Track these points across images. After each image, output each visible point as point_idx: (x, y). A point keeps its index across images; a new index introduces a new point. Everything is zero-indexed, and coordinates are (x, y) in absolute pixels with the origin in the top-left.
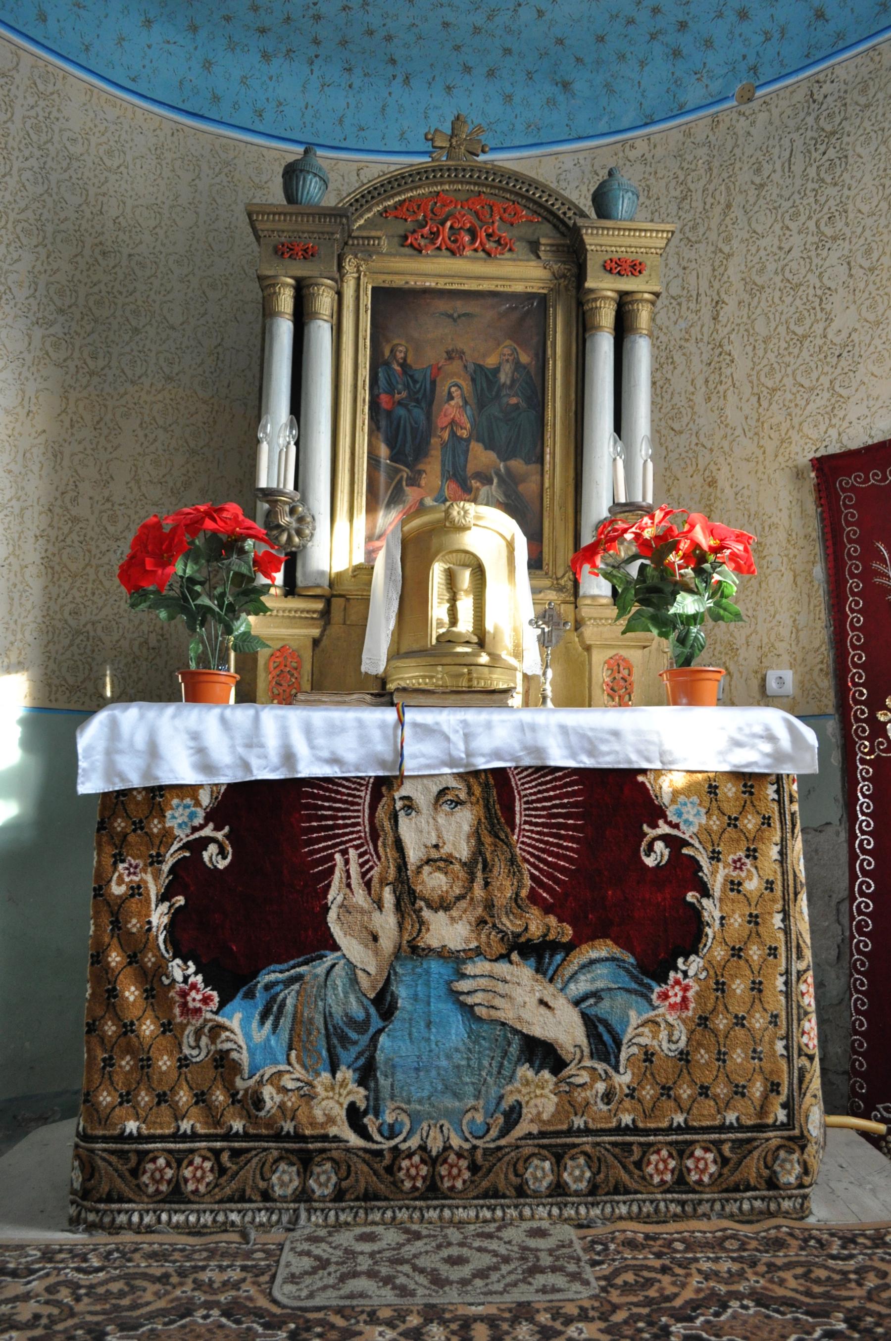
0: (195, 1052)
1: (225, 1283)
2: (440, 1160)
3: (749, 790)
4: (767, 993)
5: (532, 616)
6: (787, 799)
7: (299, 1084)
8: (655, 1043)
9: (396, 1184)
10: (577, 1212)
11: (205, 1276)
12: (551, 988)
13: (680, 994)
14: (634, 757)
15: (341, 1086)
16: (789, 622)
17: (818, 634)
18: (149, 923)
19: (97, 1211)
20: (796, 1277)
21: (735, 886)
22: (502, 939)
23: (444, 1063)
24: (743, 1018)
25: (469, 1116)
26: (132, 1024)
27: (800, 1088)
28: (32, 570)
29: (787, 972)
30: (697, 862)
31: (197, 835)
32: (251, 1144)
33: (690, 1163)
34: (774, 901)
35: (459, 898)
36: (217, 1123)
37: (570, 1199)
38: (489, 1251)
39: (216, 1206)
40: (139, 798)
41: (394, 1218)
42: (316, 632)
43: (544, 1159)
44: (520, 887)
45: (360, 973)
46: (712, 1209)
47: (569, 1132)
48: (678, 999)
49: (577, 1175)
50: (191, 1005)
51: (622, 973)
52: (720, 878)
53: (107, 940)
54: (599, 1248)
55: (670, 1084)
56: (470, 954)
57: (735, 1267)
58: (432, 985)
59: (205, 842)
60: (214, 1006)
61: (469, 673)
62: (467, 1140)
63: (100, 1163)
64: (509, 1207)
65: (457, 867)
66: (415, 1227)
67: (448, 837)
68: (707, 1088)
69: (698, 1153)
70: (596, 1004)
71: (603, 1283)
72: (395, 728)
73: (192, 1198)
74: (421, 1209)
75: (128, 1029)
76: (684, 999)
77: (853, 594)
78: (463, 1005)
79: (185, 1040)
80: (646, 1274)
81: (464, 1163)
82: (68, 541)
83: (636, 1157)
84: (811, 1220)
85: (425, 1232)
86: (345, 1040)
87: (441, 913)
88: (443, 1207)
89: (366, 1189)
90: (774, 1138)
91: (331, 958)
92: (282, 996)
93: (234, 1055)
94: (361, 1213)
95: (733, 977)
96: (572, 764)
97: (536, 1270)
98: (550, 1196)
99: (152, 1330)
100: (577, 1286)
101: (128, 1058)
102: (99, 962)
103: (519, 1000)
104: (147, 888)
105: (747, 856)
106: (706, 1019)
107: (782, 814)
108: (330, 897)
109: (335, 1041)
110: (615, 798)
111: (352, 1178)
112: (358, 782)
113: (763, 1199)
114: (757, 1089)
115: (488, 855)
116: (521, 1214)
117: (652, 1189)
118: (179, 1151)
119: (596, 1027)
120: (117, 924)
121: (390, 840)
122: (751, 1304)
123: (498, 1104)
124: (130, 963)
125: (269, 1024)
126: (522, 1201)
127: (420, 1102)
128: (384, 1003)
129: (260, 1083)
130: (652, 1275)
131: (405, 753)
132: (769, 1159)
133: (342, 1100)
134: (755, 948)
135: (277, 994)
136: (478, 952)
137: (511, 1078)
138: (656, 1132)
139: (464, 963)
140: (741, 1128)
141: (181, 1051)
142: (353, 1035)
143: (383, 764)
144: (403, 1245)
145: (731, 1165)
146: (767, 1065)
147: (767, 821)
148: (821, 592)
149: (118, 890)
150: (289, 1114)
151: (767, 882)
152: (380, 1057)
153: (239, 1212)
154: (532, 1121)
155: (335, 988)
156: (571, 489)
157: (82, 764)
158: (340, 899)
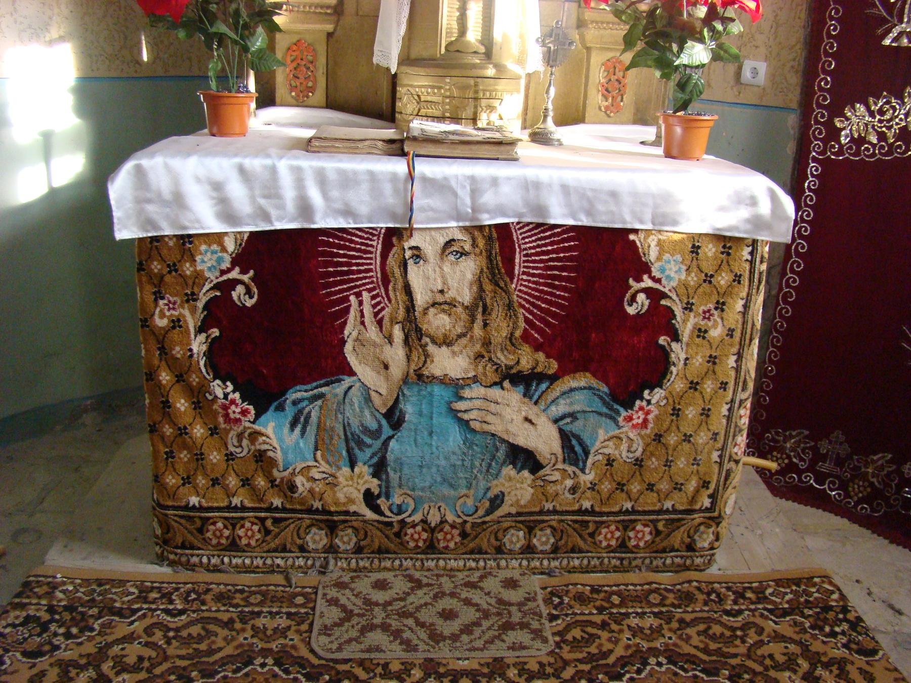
1: (275, 630)
2: (438, 529)
6: (758, 260)
7: (325, 476)
8: (617, 452)
9: (404, 545)
10: (541, 564)
11: (260, 622)
12: (535, 409)
13: (642, 417)
14: (628, 217)
18: (191, 350)
19: (176, 554)
20: (699, 633)
21: (701, 333)
22: (497, 370)
23: (443, 462)
24: (691, 436)
25: (462, 500)
26: (185, 428)
27: (725, 484)
30: (673, 311)
31: (225, 277)
32: (289, 515)
33: (632, 534)
34: (731, 345)
35: (460, 336)
36: (261, 500)
37: (536, 556)
39: (264, 555)
40: (171, 243)
41: (401, 565)
42: (330, 27)
44: (515, 328)
45: (373, 394)
46: (643, 563)
47: (541, 513)
48: (640, 421)
49: (543, 540)
50: (232, 416)
52: (689, 326)
53: (156, 362)
55: (625, 481)
56: (468, 382)
57: (656, 622)
58: (435, 404)
59: (234, 283)
60: (251, 416)
61: (476, 85)
62: (459, 517)
63: (173, 523)
64: (489, 560)
65: (460, 310)
66: (417, 575)
67: (453, 283)
68: (653, 485)
69: (639, 527)
70: (572, 422)
71: (557, 639)
72: (406, 181)
73: (246, 548)
74: (422, 560)
75: (182, 431)
76: (645, 421)
78: (460, 420)
79: (229, 441)
80: (589, 629)
81: (456, 532)
83: (591, 530)
84: (713, 570)
85: (425, 581)
86: (361, 444)
87: (444, 348)
88: (438, 559)
89: (380, 547)
90: (698, 518)
91: (348, 381)
92: (307, 410)
93: (270, 454)
94: (376, 561)
95: (688, 405)
96: (571, 222)
97: (508, 626)
98: (522, 553)
99: (225, 677)
100: (538, 644)
104: (185, 321)
105: (716, 309)
106: (661, 436)
107: (752, 272)
108: (346, 333)
109: (353, 444)
110: (603, 255)
111: (369, 539)
112: (371, 233)
113: (682, 557)
115: (488, 301)
116: (498, 565)
117: (600, 550)
118: (233, 518)
119: (570, 441)
120: (164, 351)
121: (400, 285)
122: (664, 661)
123: (485, 493)
124: (178, 381)
126: (499, 556)
127: (423, 489)
128: (394, 417)
129: (293, 474)
130: (595, 631)
132: (692, 531)
133: (359, 487)
134: (709, 382)
135: (304, 408)
136: (475, 379)
137: (497, 476)
138: (609, 514)
139: (463, 387)
140: (675, 511)
141: (227, 449)
142: (368, 440)
143: (394, 217)
144: (408, 594)
145: (662, 536)
146: (702, 469)
147: (738, 279)
150: (317, 496)
151: (729, 329)
152: (390, 457)
153: (283, 558)
154: (512, 505)
155: (352, 404)
157: (117, 214)
158: (355, 334)
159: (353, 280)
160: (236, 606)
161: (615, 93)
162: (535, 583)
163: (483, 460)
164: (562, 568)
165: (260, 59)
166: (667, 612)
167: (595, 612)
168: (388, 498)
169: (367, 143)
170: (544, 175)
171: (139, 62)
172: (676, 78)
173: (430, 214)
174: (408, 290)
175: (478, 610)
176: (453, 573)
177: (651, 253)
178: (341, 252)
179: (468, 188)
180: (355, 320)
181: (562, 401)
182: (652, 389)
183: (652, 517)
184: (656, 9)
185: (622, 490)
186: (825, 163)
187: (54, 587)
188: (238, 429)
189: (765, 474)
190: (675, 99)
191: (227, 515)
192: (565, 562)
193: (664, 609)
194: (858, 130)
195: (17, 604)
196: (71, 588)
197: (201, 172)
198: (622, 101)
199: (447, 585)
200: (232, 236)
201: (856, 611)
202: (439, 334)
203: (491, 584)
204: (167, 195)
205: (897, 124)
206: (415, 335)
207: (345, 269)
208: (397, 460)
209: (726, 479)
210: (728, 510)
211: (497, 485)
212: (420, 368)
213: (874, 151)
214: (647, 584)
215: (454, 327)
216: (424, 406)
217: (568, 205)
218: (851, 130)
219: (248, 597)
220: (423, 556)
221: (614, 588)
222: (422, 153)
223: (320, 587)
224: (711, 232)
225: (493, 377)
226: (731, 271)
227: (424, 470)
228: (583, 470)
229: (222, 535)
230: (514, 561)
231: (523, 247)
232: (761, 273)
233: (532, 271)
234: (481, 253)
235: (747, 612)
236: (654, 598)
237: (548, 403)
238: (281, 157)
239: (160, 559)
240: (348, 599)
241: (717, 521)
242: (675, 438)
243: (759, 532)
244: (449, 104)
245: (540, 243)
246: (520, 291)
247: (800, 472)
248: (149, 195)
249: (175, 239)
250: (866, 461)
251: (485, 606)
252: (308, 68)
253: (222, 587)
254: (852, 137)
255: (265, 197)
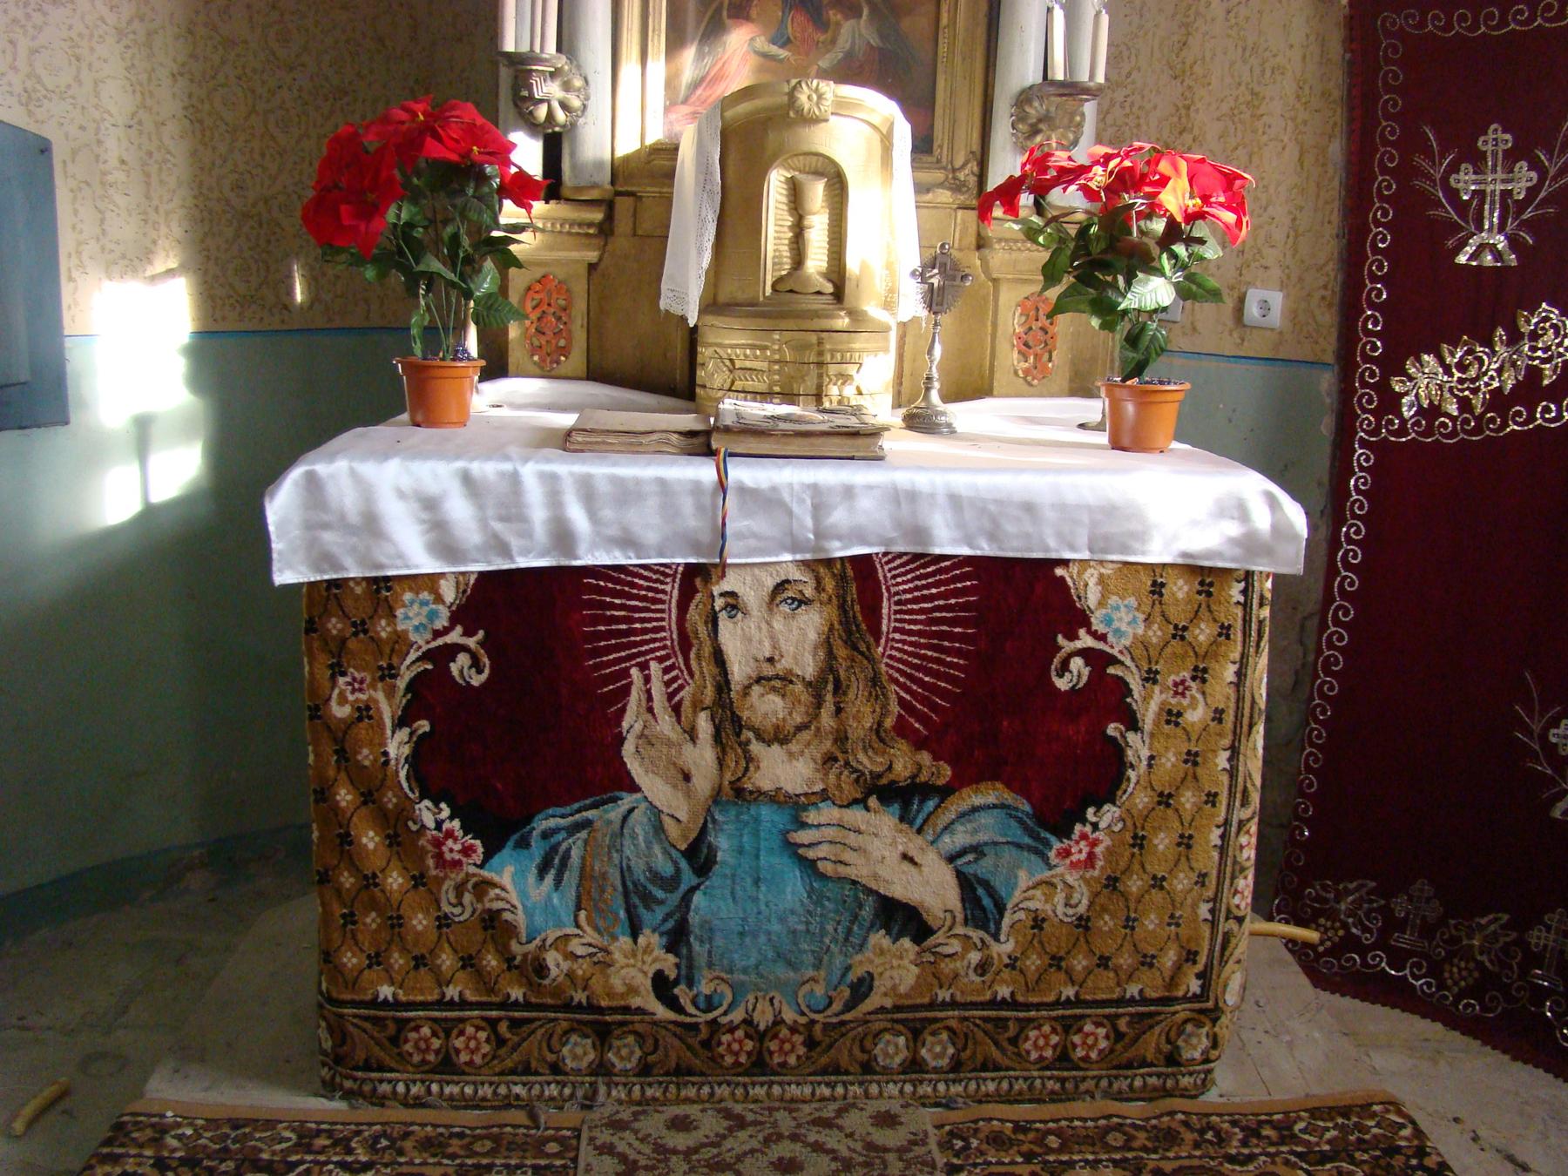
0: (457, 910)
2: (770, 1035)
3: (1206, 590)
4: (1196, 848)
5: (915, 262)
6: (1255, 602)
8: (1048, 907)
9: (716, 1060)
10: (935, 1089)
12: (919, 840)
13: (1086, 850)
14: (1052, 542)
15: (645, 952)
16: (1287, 221)
17: (1326, 247)
18: (386, 754)
19: (355, 1079)
21: (1172, 716)
22: (857, 781)
23: (776, 927)
25: (807, 987)
26: (375, 876)
27: (1222, 954)
28: (172, 128)
29: (1227, 823)
30: (1126, 684)
31: (440, 642)
32: (534, 1014)
33: (1077, 1039)
34: (1221, 735)
35: (800, 728)
36: (491, 991)
38: (827, 1152)
40: (358, 590)
41: (712, 1094)
42: (593, 256)
43: (899, 1034)
45: (667, 821)
46: (1097, 1085)
47: (932, 1006)
48: (1083, 856)
49: (938, 1050)
50: (448, 856)
51: (1013, 823)
52: (1154, 706)
53: (331, 773)
54: (959, 1144)
55: (1062, 953)
56: (813, 799)
59: (453, 651)
60: (478, 857)
61: (820, 343)
62: (803, 1014)
63: (351, 1028)
65: (799, 687)
66: (738, 1108)
67: (788, 648)
68: (1108, 959)
69: (1088, 1028)
70: (976, 860)
72: (714, 494)
73: (467, 1069)
74: (745, 1086)
75: (370, 881)
76: (1091, 856)
77: (1382, 198)
81: (798, 1039)
82: (221, 78)
84: (1212, 1096)
85: (750, 1117)
86: (648, 900)
88: (771, 1084)
90: (1182, 1011)
91: (628, 800)
92: (564, 846)
93: (507, 916)
94: (672, 1088)
96: (965, 551)
98: (904, 1073)
101: (373, 914)
102: (325, 800)
103: (876, 854)
104: (378, 709)
105: (1194, 678)
106: (1116, 879)
108: (625, 725)
109: (635, 900)
110: (1014, 601)
111: (660, 1052)
112: (662, 571)
113: (1159, 1075)
114: (1169, 958)
115: (842, 673)
118: (446, 1019)
120: (342, 754)
121: (707, 650)
123: (844, 975)
124: (365, 803)
125: (550, 878)
127: (745, 971)
128: (699, 856)
129: (542, 947)
131: (728, 531)
133: (646, 968)
134: (1189, 794)
135: (559, 844)
136: (824, 795)
137: (861, 947)
138: (1038, 1006)
139: (805, 808)
140: (1144, 1001)
141: (439, 908)
142: (660, 894)
143: (696, 548)
144: (724, 1137)
145: (1127, 1040)
147: (1225, 631)
148: (1336, 183)
149: (341, 712)
150: (580, 983)
151: (1216, 710)
152: (694, 919)
153: (524, 1084)
154: (886, 994)
155: (634, 836)
156: (981, 32)
157: (277, 546)
158: (638, 727)
159: (636, 644)
160: (453, 1156)
161: (1038, 349)
162: (924, 1119)
163: (839, 923)
164: (968, 1096)
165: (489, 308)
166: (1135, 1158)
167: (1020, 1160)
168: (690, 984)
169: (655, 437)
170: (922, 481)
171: (286, 305)
172: (1123, 328)
173: (752, 542)
174: (719, 658)
175: (835, 1159)
176: (793, 1106)
177: (1090, 595)
178: (617, 601)
179: (809, 502)
180: (639, 705)
181: (959, 828)
182: (1099, 807)
183: (1107, 1011)
184: (1090, 226)
185: (1059, 968)
186: (1380, 449)
187: (163, 1130)
188: (456, 877)
189: (1307, 955)
190: (1124, 361)
191: (437, 1014)
192: (973, 1086)
193: (1130, 1155)
194: (1429, 396)
195: (108, 1155)
196: (189, 1132)
197: (406, 483)
198: (1050, 360)
199: (785, 1122)
200: (452, 579)
201: (1439, 1154)
202: (768, 725)
203: (853, 1120)
204: (354, 517)
205: (1487, 385)
206: (731, 728)
207: (624, 627)
208: (705, 924)
209: (1224, 948)
210: (1231, 998)
211: (861, 962)
212: (739, 779)
213: (1454, 425)
214: (1104, 1118)
215: (790, 714)
216: (745, 839)
217: (960, 525)
218: (1417, 395)
219: (471, 1143)
220: (747, 1079)
221: (1051, 1125)
222: (738, 450)
223: (585, 1128)
224: (1180, 561)
225: (851, 791)
226: (1215, 620)
227: (748, 940)
228: (996, 937)
229: (428, 1048)
230: (891, 1085)
231: (893, 590)
232: (1261, 623)
233: (907, 627)
234: (830, 599)
235: (1263, 1158)
236: (1115, 1139)
237: (938, 829)
238: (526, 460)
239: (329, 1088)
240: (630, 1145)
241: (1213, 1015)
242: (1139, 883)
243: (1288, 1038)
244: (779, 372)
245: (919, 583)
246: (890, 657)
247: (1363, 951)
248: (326, 518)
249: (364, 584)
250: (1470, 927)
251: (845, 1153)
252: (559, 319)
253: (429, 1128)
254: (1420, 406)
255: (502, 519)
